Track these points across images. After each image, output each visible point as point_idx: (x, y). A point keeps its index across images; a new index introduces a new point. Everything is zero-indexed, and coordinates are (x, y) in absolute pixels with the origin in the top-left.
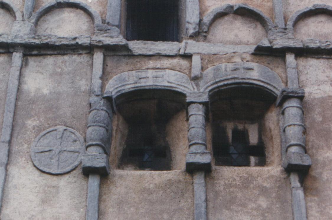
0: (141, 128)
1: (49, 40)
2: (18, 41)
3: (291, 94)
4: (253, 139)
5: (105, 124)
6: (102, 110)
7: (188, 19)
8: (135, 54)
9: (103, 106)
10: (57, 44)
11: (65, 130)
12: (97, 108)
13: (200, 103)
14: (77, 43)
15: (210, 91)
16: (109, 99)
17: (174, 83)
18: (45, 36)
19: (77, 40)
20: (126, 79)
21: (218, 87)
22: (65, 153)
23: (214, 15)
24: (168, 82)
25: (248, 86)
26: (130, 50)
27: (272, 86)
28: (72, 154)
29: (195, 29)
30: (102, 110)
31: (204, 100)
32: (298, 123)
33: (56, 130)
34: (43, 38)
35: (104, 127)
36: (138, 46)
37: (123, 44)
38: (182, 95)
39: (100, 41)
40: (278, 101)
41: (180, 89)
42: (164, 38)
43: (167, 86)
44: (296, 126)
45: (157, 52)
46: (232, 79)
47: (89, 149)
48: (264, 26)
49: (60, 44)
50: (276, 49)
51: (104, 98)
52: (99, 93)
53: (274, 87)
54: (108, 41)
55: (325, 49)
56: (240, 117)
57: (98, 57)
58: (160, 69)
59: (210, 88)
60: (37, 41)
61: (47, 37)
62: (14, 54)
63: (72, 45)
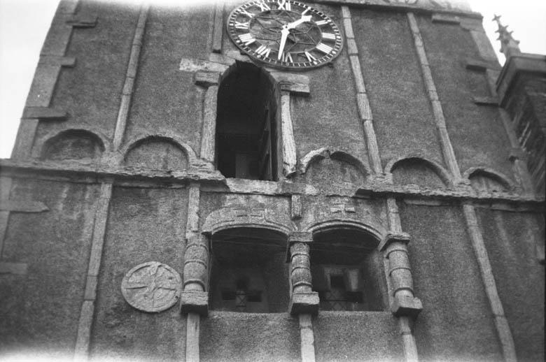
0: (243, 269)
1: (142, 172)
2: (109, 171)
5: (204, 260)
6: (201, 245)
7: (286, 159)
9: (203, 241)
11: (160, 266)
13: (304, 243)
14: (172, 176)
15: (313, 231)
16: (207, 235)
18: (138, 168)
21: (320, 229)
22: (161, 290)
25: (330, 229)
26: (228, 187)
28: (167, 291)
29: (292, 170)
31: (308, 240)
32: (404, 267)
33: (149, 266)
34: (136, 170)
35: (203, 264)
39: (196, 176)
40: (382, 244)
42: (262, 177)
43: (266, 226)
44: (143, 315)
48: (357, 169)
50: (496, 199)
51: (203, 233)
52: (196, 229)
53: (378, 232)
54: (204, 176)
55: (425, 196)
56: (345, 261)
57: (195, 192)
59: (314, 228)
62: (103, 185)
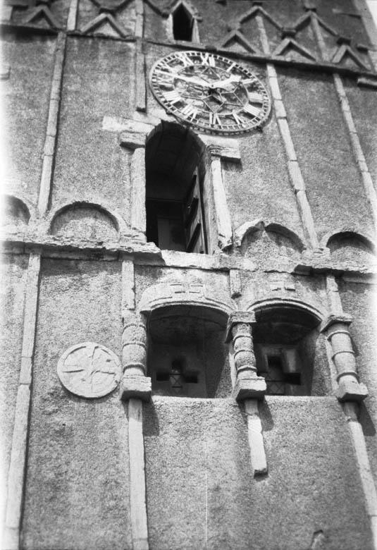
1: (72, 242)
3: (339, 319)
4: (291, 365)
6: (140, 326)
8: (168, 265)
10: (81, 247)
12: (135, 323)
14: (104, 248)
17: (213, 301)
19: (104, 245)
20: (160, 293)
23: (100, 206)
24: (207, 299)
26: (163, 261)
27: (315, 309)
29: (228, 242)
30: (140, 326)
33: (85, 347)
36: (169, 257)
37: (155, 252)
38: (223, 315)
39: (129, 248)
40: (323, 326)
41: (222, 308)
45: (191, 264)
46: (284, 300)
47: (127, 371)
49: (85, 247)
53: (318, 311)
58: (186, 280)
60: (59, 244)
61: (69, 240)
63: (98, 250)
